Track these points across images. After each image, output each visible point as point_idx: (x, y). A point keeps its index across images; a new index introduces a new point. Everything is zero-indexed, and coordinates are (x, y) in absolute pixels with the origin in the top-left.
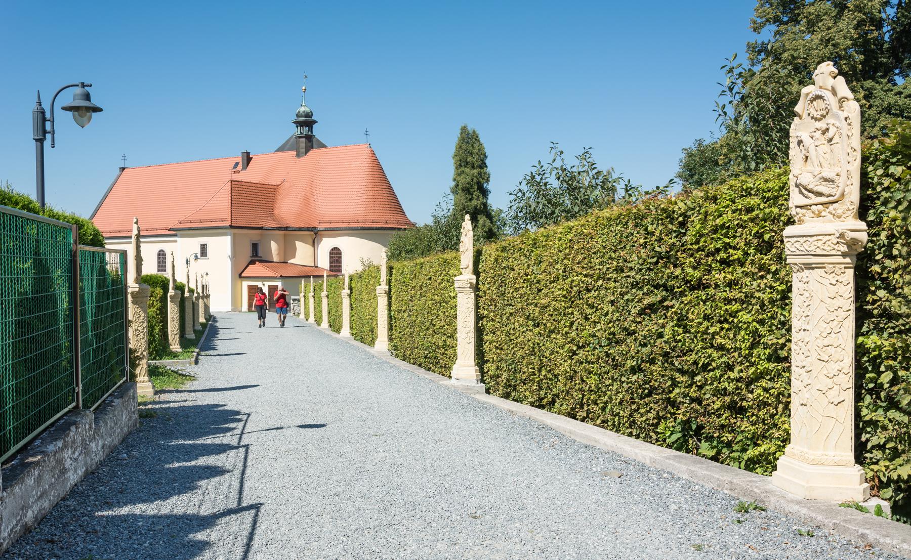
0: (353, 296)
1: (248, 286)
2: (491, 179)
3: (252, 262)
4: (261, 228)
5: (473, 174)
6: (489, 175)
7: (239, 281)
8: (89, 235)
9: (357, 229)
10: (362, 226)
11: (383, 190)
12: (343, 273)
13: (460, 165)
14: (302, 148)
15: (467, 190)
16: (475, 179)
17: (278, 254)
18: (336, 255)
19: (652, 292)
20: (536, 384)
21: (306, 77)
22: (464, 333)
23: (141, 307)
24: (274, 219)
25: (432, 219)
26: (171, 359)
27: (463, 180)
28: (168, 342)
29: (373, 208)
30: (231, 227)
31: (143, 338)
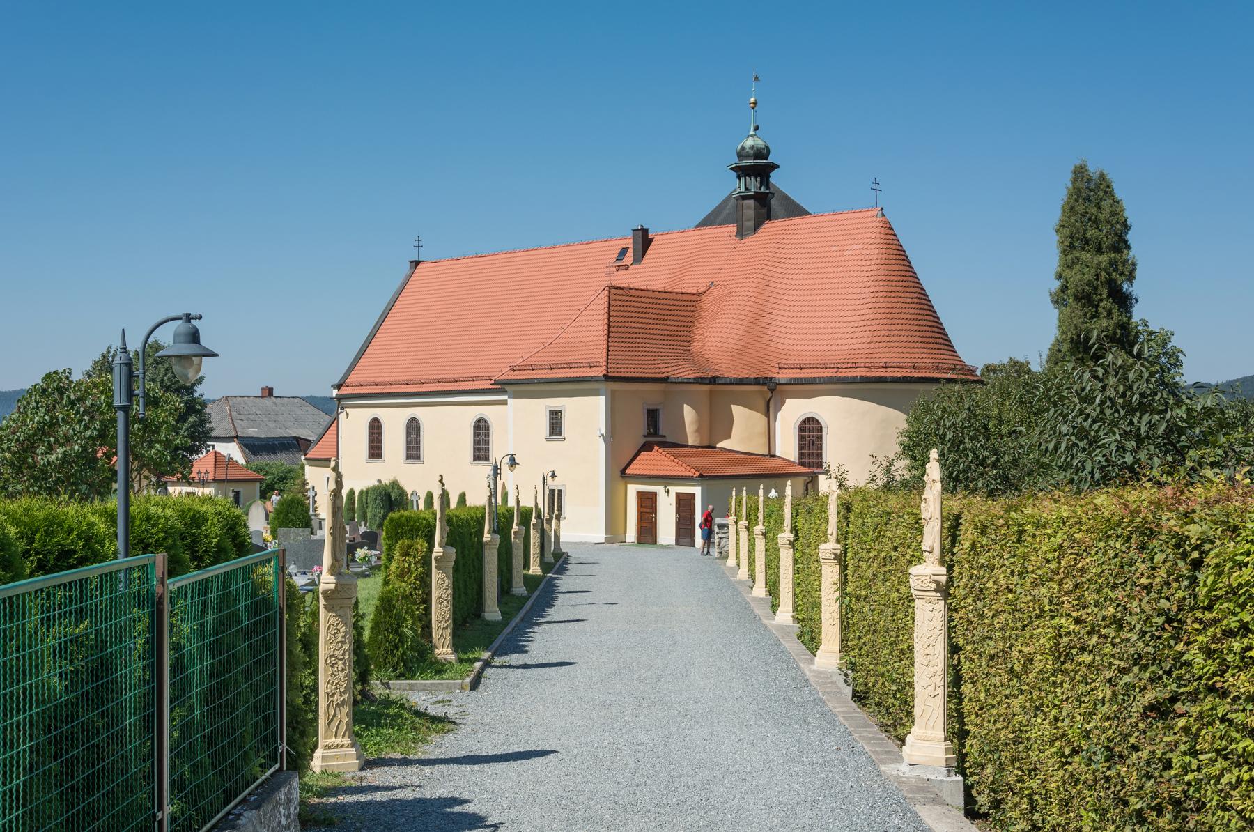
0: (798, 546)
1: (694, 494)
2: (1137, 274)
3: (647, 447)
4: (665, 380)
5: (1098, 265)
6: (1134, 264)
7: (621, 486)
8: (214, 536)
9: (853, 381)
10: (863, 374)
11: (909, 300)
13: (1072, 247)
14: (749, 220)
15: (1086, 298)
16: (1103, 273)
17: (698, 431)
18: (810, 432)
19: (1160, 678)
20: (1025, 800)
21: (756, 78)
22: (924, 677)
23: (340, 616)
24: (689, 362)
25: (1008, 359)
26: (431, 678)
27: (1077, 277)
28: (431, 642)
29: (887, 339)
30: (607, 378)
31: (343, 670)
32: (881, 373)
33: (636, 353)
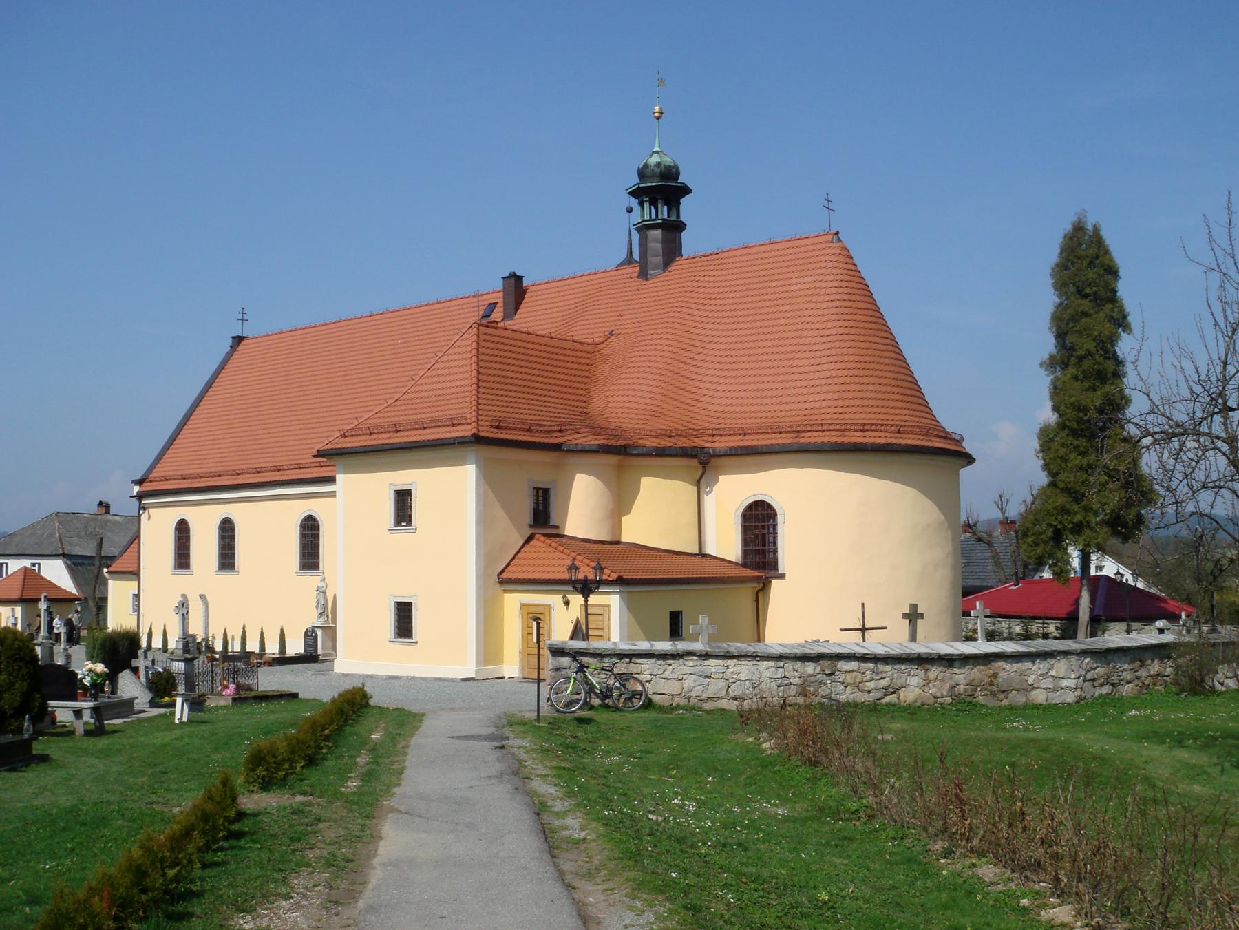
21: (661, 82)
32: (857, 438)
33: (517, 410)
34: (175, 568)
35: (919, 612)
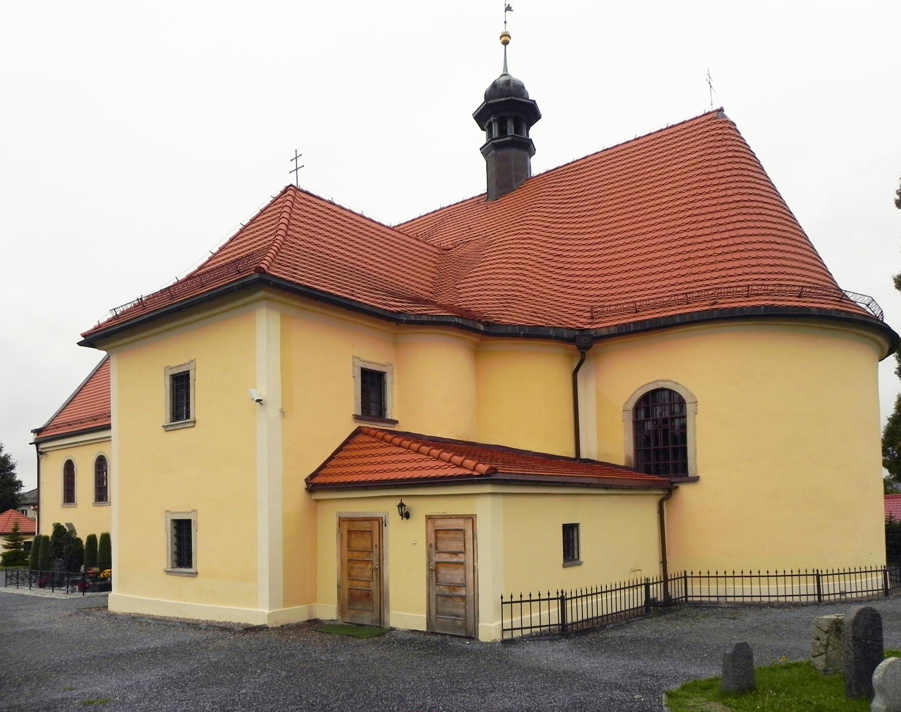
12: (691, 474)
34: (65, 502)
35: (423, 628)
